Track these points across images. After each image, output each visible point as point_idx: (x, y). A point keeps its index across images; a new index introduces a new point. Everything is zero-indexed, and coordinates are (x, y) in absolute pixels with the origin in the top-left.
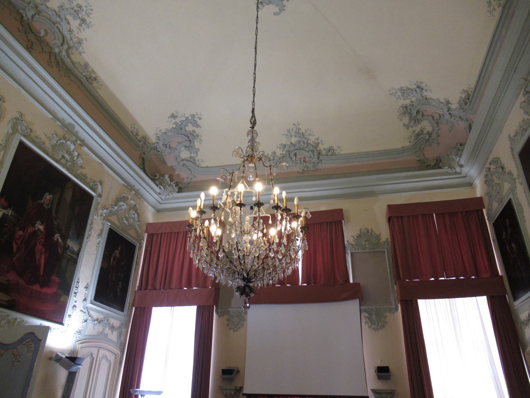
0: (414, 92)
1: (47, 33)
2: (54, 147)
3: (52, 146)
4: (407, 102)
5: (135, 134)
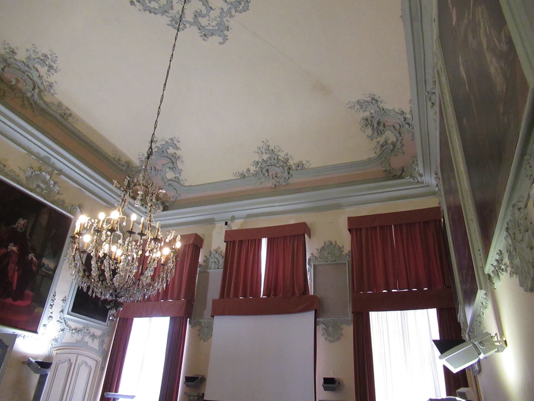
0: (371, 104)
1: (18, 81)
2: (28, 178)
3: (26, 178)
4: (367, 114)
5: (117, 160)
